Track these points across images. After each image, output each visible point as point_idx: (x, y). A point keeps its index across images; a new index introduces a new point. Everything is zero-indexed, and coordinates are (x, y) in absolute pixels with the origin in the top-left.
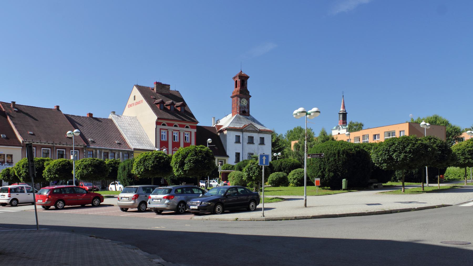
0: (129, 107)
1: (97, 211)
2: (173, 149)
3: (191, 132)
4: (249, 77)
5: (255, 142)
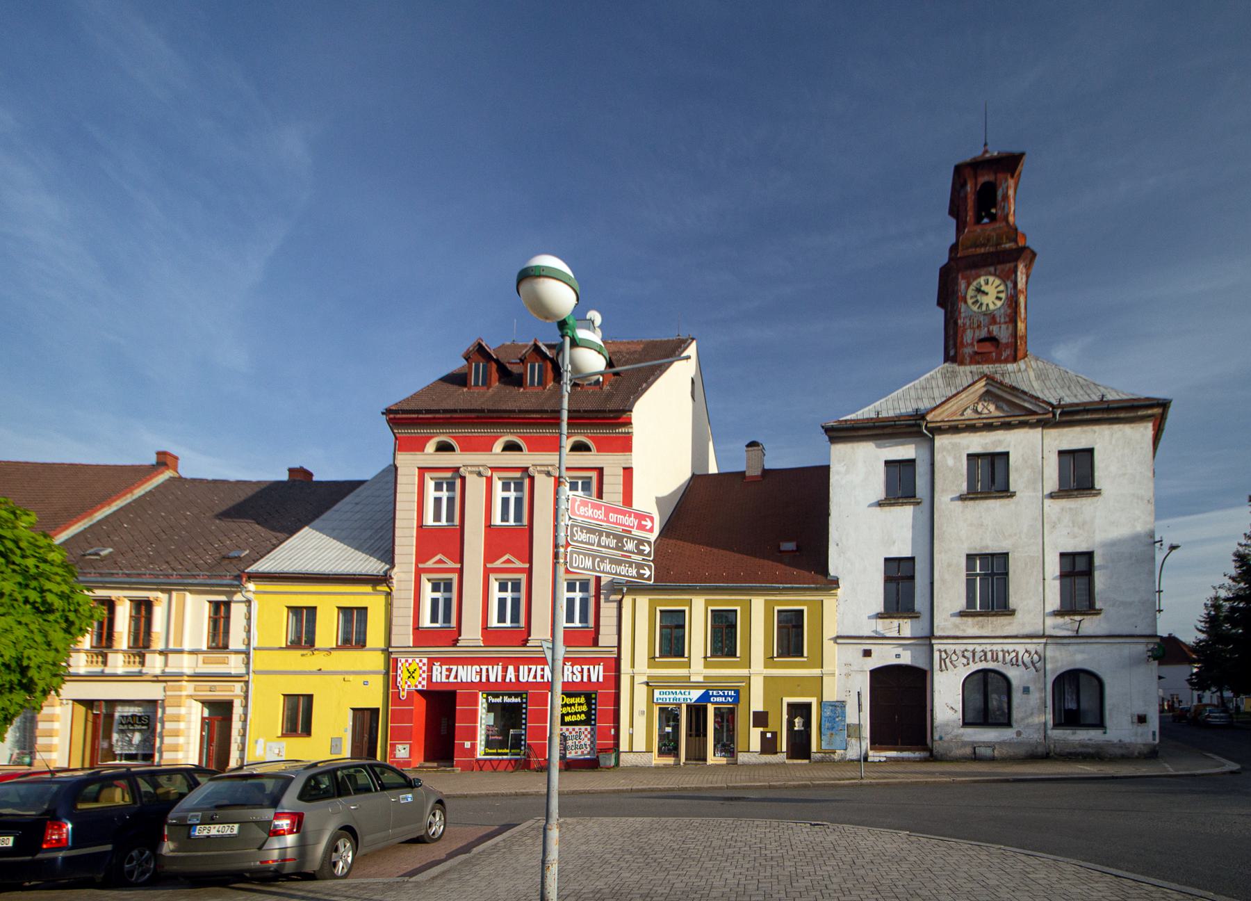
1: (287, 545)
3: (600, 471)
4: (1021, 155)
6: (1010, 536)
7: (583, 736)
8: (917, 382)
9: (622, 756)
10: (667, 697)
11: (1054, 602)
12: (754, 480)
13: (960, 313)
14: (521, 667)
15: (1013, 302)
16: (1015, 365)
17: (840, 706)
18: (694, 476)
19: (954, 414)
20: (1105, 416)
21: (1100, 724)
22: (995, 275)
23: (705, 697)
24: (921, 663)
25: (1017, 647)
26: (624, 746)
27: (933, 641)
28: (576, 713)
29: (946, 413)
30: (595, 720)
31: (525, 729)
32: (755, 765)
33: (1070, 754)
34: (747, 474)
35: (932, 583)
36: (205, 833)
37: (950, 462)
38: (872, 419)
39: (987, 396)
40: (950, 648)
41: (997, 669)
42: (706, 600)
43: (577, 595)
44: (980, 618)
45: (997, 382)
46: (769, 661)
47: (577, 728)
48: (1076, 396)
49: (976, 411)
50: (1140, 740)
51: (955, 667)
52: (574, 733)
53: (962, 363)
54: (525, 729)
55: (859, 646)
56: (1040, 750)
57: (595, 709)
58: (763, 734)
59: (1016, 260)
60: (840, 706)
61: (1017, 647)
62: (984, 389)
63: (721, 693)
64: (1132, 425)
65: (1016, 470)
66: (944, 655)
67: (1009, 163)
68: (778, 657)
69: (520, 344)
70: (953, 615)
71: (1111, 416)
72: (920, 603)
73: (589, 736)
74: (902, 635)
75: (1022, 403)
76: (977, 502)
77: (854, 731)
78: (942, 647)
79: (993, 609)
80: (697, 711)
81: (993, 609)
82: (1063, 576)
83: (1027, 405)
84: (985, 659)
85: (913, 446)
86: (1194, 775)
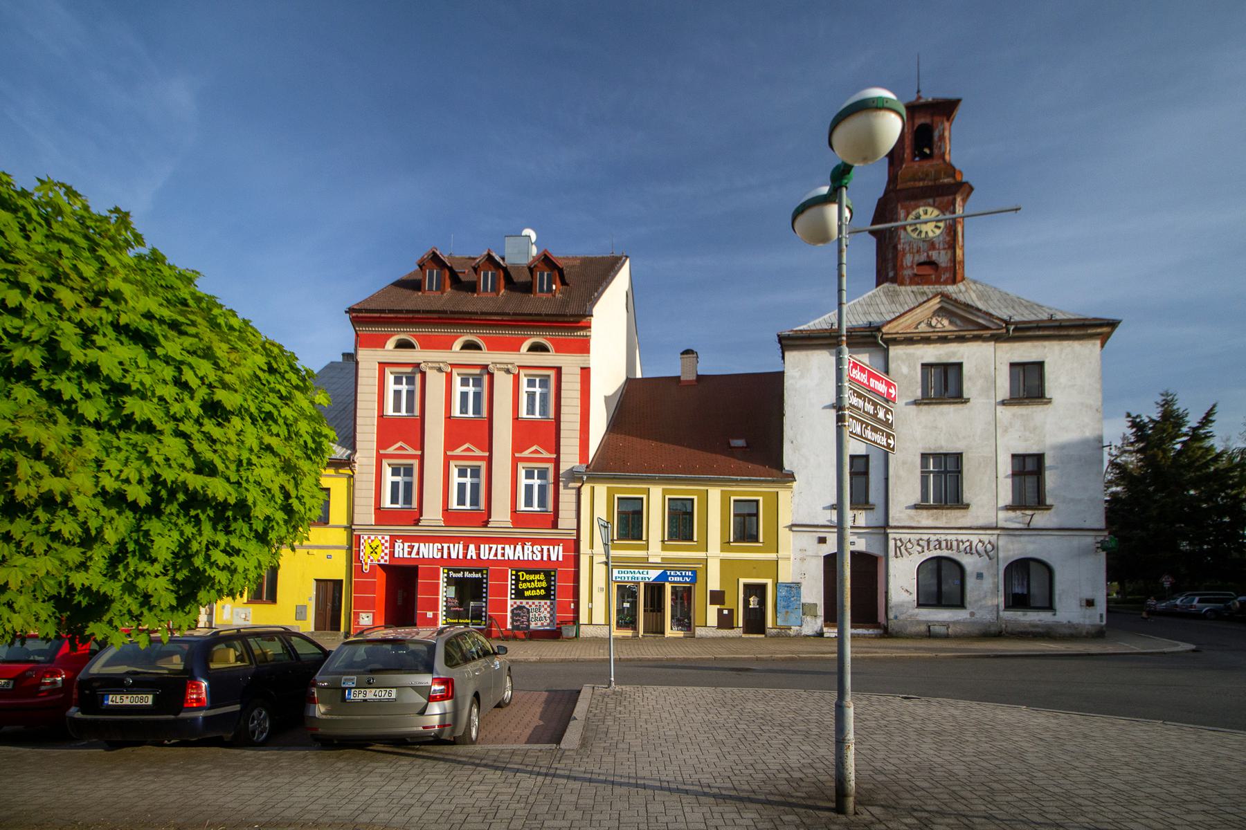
0: (780, 341)
2: (449, 453)
3: (558, 370)
5: (968, 389)
6: (964, 438)
7: (542, 609)
8: (861, 299)
9: (582, 628)
10: (626, 575)
11: (1006, 497)
12: (689, 384)
13: (900, 239)
14: (482, 546)
15: (951, 231)
16: (955, 287)
17: (795, 587)
18: (627, 379)
19: (909, 327)
20: (1056, 333)
21: (1050, 607)
22: (933, 206)
23: (664, 577)
24: (876, 550)
25: (972, 538)
26: (583, 618)
27: (889, 531)
28: (535, 589)
29: (901, 327)
30: (554, 595)
31: (486, 602)
32: (714, 639)
33: (1022, 633)
34: (682, 379)
35: (887, 479)
36: (361, 697)
37: (905, 370)
38: (826, 330)
39: (941, 312)
40: (905, 537)
41: (952, 556)
42: (663, 489)
43: (536, 482)
44: (935, 511)
45: (951, 299)
46: (725, 545)
47: (537, 602)
48: (1022, 315)
49: (930, 325)
50: (1087, 622)
51: (910, 554)
52: (533, 606)
53: (902, 283)
54: (486, 602)
55: (814, 534)
56: (993, 629)
57: (554, 586)
58: (720, 611)
59: (955, 193)
60: (795, 587)
61: (972, 538)
62: (939, 306)
63: (678, 573)
64: (1081, 342)
65: (970, 379)
66: (899, 543)
67: (946, 108)
68: (734, 541)
69: (457, 256)
70: (908, 508)
71: (1062, 333)
72: (875, 496)
73: (548, 609)
74: (857, 524)
75: (976, 319)
76: (932, 406)
77: (808, 609)
78: (898, 536)
79: (946, 502)
80: (655, 591)
81: (946, 502)
82: (1014, 475)
83: (980, 321)
84: (940, 548)
85: (867, 355)
86: (1164, 653)
